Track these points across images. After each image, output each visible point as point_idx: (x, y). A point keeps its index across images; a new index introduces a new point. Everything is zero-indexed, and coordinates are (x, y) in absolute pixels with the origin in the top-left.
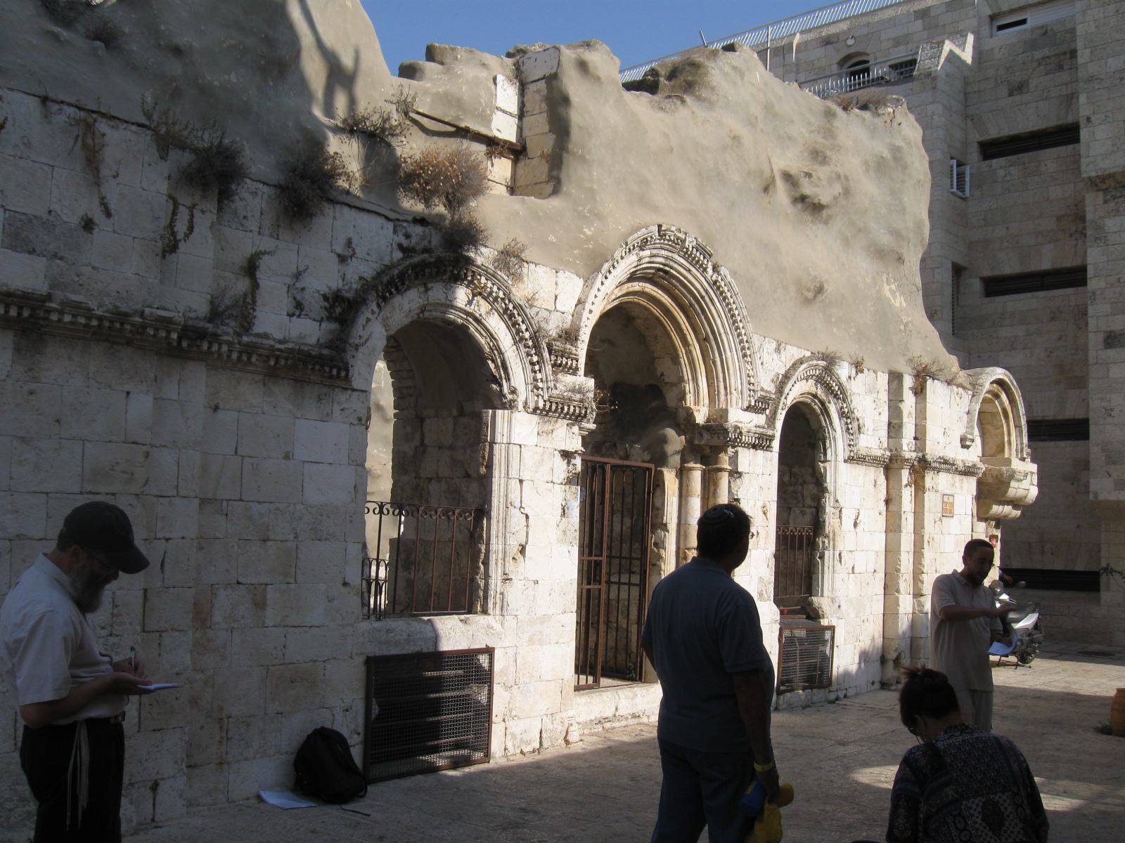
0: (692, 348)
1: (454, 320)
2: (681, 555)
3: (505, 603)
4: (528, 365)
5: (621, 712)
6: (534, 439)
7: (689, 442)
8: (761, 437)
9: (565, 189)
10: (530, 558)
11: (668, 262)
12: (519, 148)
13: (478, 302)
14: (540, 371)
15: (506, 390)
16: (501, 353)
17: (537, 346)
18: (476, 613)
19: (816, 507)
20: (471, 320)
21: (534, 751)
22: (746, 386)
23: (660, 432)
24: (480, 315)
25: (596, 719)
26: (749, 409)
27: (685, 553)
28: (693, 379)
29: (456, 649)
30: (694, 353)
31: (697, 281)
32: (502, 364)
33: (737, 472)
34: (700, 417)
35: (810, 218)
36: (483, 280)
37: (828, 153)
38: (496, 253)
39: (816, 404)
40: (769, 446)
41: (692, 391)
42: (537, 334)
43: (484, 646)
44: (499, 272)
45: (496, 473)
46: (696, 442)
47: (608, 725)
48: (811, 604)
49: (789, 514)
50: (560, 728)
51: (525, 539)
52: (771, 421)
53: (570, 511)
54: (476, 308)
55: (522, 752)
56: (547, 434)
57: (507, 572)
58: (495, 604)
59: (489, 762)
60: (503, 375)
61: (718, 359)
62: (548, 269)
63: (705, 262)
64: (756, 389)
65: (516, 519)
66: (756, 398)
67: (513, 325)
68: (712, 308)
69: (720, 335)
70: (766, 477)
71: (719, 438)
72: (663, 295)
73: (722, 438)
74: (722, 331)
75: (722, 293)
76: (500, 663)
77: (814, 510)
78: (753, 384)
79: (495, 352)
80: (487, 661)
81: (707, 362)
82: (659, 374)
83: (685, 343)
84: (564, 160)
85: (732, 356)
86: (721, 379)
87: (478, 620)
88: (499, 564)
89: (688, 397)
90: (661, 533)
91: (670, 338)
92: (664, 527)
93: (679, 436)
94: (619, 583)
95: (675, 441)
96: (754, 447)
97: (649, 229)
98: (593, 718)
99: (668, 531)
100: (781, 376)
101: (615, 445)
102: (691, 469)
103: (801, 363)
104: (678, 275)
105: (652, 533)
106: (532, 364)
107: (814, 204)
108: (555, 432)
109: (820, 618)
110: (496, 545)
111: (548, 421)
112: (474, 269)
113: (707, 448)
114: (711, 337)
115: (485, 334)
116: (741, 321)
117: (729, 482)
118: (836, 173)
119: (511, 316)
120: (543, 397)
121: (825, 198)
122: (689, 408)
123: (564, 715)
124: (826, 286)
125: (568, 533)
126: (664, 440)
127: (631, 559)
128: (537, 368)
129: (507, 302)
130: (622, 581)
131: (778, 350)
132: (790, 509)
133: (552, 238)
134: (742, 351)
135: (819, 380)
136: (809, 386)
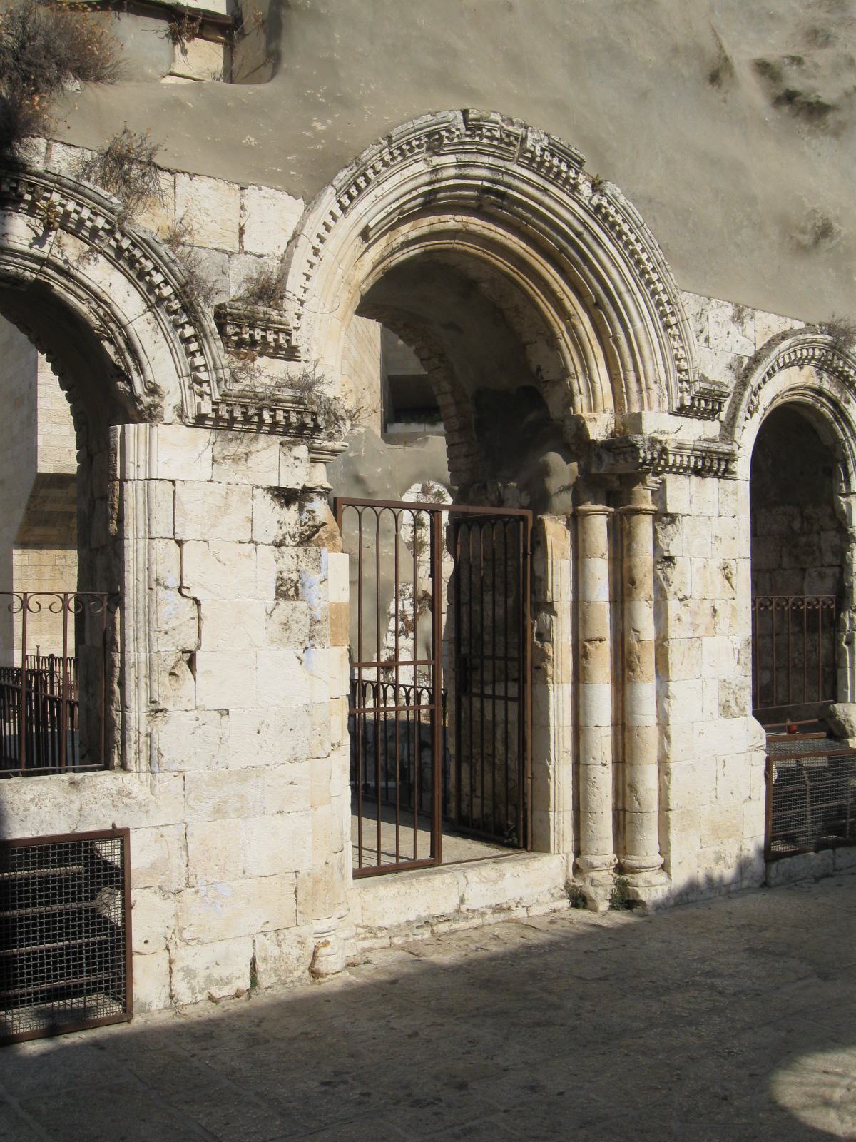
0: (577, 322)
1: (18, 275)
2: (581, 652)
3: (155, 753)
4: (178, 344)
5: (472, 903)
6: (206, 470)
7: (584, 471)
8: (706, 455)
9: (285, 65)
11: (499, 177)
12: (230, 22)
13: (58, 239)
14: (201, 351)
15: (139, 389)
16: (121, 326)
17: (189, 309)
18: (112, 768)
20: (50, 272)
21: (238, 995)
23: (541, 460)
24: (66, 262)
25: (419, 918)
26: (681, 411)
27: (585, 647)
28: (584, 371)
29: (41, 834)
30: (580, 327)
31: (565, 209)
32: (127, 344)
33: (667, 515)
34: (599, 428)
35: (805, 127)
36: (56, 197)
37: (833, 30)
38: (96, 155)
39: (823, 405)
40: (726, 470)
41: (583, 389)
42: (188, 289)
43: (108, 827)
44: (85, 183)
45: (130, 532)
46: (594, 471)
47: (443, 928)
48: (833, 715)
49: (804, 578)
50: (296, 952)
51: (194, 639)
52: (728, 429)
53: (307, 591)
54: (55, 250)
55: (211, 998)
56: (236, 459)
57: (156, 698)
58: (138, 753)
60: (131, 364)
61: (621, 335)
62: (221, 184)
63: (572, 174)
65: (171, 609)
67: (139, 277)
69: (620, 295)
70: (727, 520)
71: (625, 459)
72: (509, 235)
73: (630, 460)
74: (622, 288)
75: (613, 225)
76: (142, 857)
77: (837, 570)
78: (686, 371)
79: (112, 325)
80: (117, 851)
82: (534, 369)
83: (564, 314)
84: (284, 21)
85: (643, 325)
86: (630, 367)
87: (104, 781)
88: (142, 685)
89: (577, 399)
90: (545, 616)
92: (550, 608)
93: (568, 461)
94: (494, 697)
95: (562, 471)
96: (697, 472)
97: (440, 115)
98: (413, 918)
99: (555, 614)
100: (746, 361)
101: (485, 487)
102: (587, 514)
103: (783, 339)
104: (524, 199)
106: (186, 341)
107: (810, 104)
108: (252, 458)
110: (135, 654)
111: (237, 438)
112: (33, 179)
113: (614, 478)
115: (85, 296)
116: (653, 270)
117: (655, 531)
119: (132, 261)
120: (210, 395)
121: (828, 94)
122: (580, 417)
123: (304, 930)
125: (294, 626)
126: (545, 471)
127: (506, 658)
129: (118, 236)
130: (497, 694)
131: (738, 318)
132: (804, 570)
133: (251, 140)
135: (823, 366)
136: (806, 376)
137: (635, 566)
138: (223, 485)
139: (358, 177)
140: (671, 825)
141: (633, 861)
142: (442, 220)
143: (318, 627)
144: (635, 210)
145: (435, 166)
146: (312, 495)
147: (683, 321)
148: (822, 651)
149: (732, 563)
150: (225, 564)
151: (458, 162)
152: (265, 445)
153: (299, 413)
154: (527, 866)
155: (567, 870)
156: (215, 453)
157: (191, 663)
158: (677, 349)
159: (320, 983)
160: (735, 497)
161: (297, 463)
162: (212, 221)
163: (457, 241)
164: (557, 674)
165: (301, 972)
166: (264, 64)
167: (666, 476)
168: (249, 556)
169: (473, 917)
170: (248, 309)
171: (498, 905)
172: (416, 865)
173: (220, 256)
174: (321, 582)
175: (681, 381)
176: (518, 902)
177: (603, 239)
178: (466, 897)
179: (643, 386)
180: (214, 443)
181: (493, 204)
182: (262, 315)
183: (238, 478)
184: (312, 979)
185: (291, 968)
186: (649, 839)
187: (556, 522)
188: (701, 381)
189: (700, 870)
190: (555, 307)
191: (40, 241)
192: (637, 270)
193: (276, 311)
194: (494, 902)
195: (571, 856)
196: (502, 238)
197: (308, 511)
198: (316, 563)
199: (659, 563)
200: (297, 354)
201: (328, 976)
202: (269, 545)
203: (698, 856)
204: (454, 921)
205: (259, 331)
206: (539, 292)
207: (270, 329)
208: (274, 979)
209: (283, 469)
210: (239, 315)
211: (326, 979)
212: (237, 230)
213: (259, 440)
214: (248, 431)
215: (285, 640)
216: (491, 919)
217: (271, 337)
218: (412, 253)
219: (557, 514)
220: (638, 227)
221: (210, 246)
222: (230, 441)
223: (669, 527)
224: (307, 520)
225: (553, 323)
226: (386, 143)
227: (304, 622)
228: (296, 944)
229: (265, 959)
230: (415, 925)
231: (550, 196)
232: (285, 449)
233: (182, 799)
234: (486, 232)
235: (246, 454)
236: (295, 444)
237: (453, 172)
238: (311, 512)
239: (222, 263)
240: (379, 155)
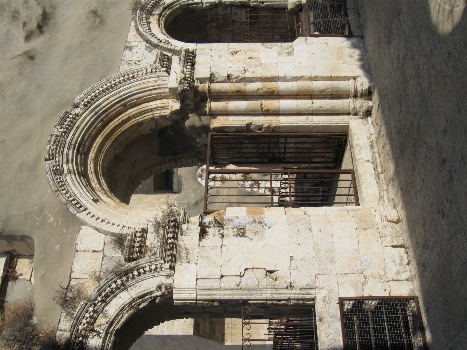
0: (132, 114)
1: (112, 343)
2: (267, 113)
3: (308, 287)
4: (141, 277)
5: (369, 157)
6: (192, 266)
7: (192, 111)
8: (186, 61)
10: (275, 265)
11: (72, 146)
13: (98, 326)
14: (144, 268)
15: (159, 293)
16: (133, 300)
17: (126, 273)
18: (314, 304)
19: (231, 7)
20: (111, 329)
21: (407, 253)
22: (153, 75)
24: (107, 323)
25: (375, 179)
26: (168, 72)
27: (264, 111)
28: (152, 111)
29: (341, 333)
30: (134, 113)
31: (85, 119)
32: (141, 298)
33: (211, 77)
34: (175, 105)
36: (81, 327)
37: (12, 9)
38: (63, 311)
39: (166, 13)
40: (192, 53)
41: (159, 112)
42: (118, 273)
43: (338, 306)
45: (218, 297)
46: (192, 107)
47: (379, 169)
48: (292, 10)
49: (237, 21)
50: (389, 229)
51: (261, 271)
52: (176, 52)
54: (102, 327)
55: (408, 264)
56: (188, 254)
57: (285, 286)
58: (308, 294)
59: (418, 297)
60: (149, 296)
62: (75, 260)
63: (71, 116)
64: (155, 67)
65: (249, 280)
67: (113, 293)
69: (121, 97)
71: (188, 94)
72: (96, 142)
73: (188, 93)
74: (118, 96)
75: (92, 99)
77: (233, 8)
78: (152, 69)
79: (133, 304)
80: (348, 302)
81: (139, 103)
82: (151, 131)
83: (129, 119)
84: (8, 234)
85: (133, 87)
86: (150, 92)
87: (319, 308)
88: (280, 292)
89: (163, 114)
90: (252, 127)
91: (125, 131)
92: (248, 125)
93: (189, 118)
94: (285, 148)
96: (193, 65)
98: (375, 181)
99: (251, 123)
100: (148, 45)
101: (199, 152)
102: (210, 110)
103: (138, 30)
104: (81, 136)
105: (253, 131)
106: (139, 274)
107: (43, 19)
108: (187, 247)
109: (301, 3)
110: (267, 295)
111: (179, 253)
112: (73, 337)
113: (196, 99)
114: (123, 102)
115: (121, 315)
117: (217, 82)
118: (23, 4)
119: (107, 296)
120: (162, 264)
121: (39, 12)
122: (171, 113)
123: (380, 226)
124: (92, 8)
125: (256, 230)
126: (193, 127)
127: (269, 143)
128: (142, 271)
129: (96, 302)
131: (130, 48)
132: (233, 21)
133: (57, 248)
135: (150, 13)
136: (154, 20)
139: (73, 204)
141: (352, 91)
142: (90, 169)
143: (256, 220)
144: (86, 90)
145: (68, 172)
146: (202, 223)
148: (266, 14)
149: (230, 51)
151: (66, 163)
152: (182, 242)
153: (169, 228)
155: (356, 118)
157: (271, 272)
158: (143, 73)
159: (402, 219)
160: (203, 49)
161: (189, 228)
163: (99, 163)
165: (397, 227)
166: (26, 242)
167: (195, 78)
168: (228, 248)
169: (375, 156)
171: (370, 146)
173: (105, 260)
174: (238, 219)
175: (156, 72)
176: (369, 138)
178: (367, 160)
179: (158, 87)
180: (181, 263)
181: (83, 149)
182: (129, 243)
183: (196, 253)
184: (400, 223)
185: (396, 231)
187: (213, 123)
188: (156, 63)
190: (126, 123)
191: (98, 334)
192: (111, 90)
193: (127, 237)
194: (369, 148)
196: (97, 145)
197: (209, 224)
198: (230, 221)
199: (230, 81)
200: (145, 229)
201: (399, 216)
202: (223, 240)
203: (350, 65)
205: (135, 244)
206: (120, 130)
207: (134, 240)
208: (400, 238)
209: (192, 234)
215: (262, 234)
217: (138, 239)
218: (104, 182)
221: (101, 264)
222: (180, 256)
224: (213, 224)
225: (132, 124)
226: (58, 192)
227: (255, 226)
228: (386, 229)
229: (392, 242)
230: (378, 180)
231: (80, 125)
232: (184, 233)
233: (327, 276)
234: (95, 151)
235: (186, 249)
236: (181, 229)
237: (70, 165)
238: (209, 223)
240: (63, 195)
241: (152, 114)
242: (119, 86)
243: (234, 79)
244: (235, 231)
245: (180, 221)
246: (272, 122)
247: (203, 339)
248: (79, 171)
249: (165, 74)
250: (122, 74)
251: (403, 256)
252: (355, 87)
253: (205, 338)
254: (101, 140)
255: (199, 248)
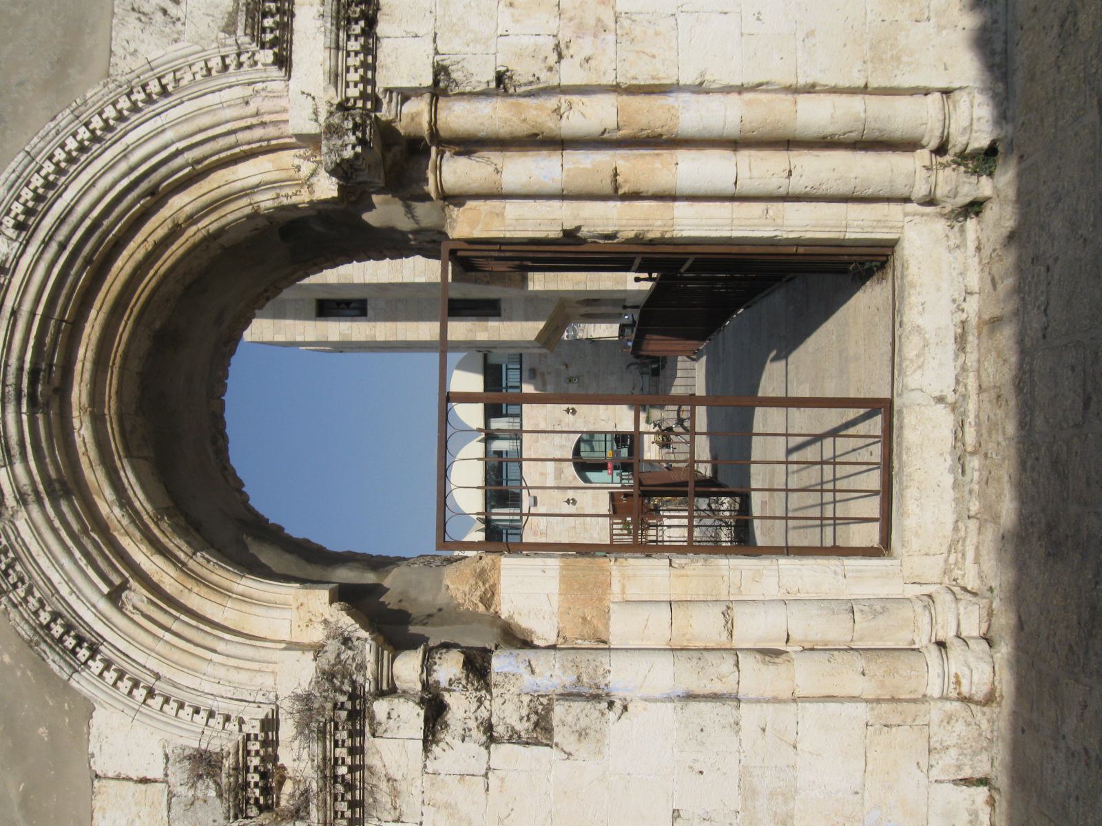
5: (945, 385)
22: (233, 77)
25: (952, 470)
26: (283, 62)
33: (436, 82)
47: (970, 436)
50: (959, 727)
56: (395, 793)
62: (97, 803)
66: (254, 47)
68: (80, 209)
69: (132, 169)
74: (123, 167)
78: (223, 58)
83: (176, 231)
86: (231, 139)
108: (394, 773)
111: (372, 792)
113: (390, 156)
114: (144, 186)
125: (583, 723)
134: (154, 102)
137: (511, 134)
138: (425, 809)
139: (52, 637)
140: (889, 86)
142: (83, 449)
144: (9, 169)
145: (18, 501)
146: (431, 682)
147: (152, 69)
150: (512, 810)
151: (5, 466)
152: (377, 757)
153: (336, 728)
154: (913, 286)
155: (927, 215)
156: (390, 818)
158: (194, 74)
159: (1001, 696)
161: (394, 715)
162: (140, 817)
163: (106, 411)
164: (660, 226)
165: (982, 717)
167: (379, 90)
168: (502, 780)
169: (965, 386)
170: (226, 796)
171: (956, 339)
172: (888, 437)
173: (176, 809)
174: (533, 672)
175: (240, 65)
176: (958, 307)
177: (60, 210)
178: (937, 394)
179: (254, 121)
180: (379, 820)
181: (48, 381)
182: (232, 779)
183: (416, 791)
184: (994, 705)
185: (976, 734)
186: (900, 116)
187: (455, 221)
188: (235, 33)
189: (960, 26)
190: (167, 247)
192: (94, 148)
193: (224, 761)
194: (951, 347)
195: (910, 207)
196: (89, 349)
197: (450, 685)
198: (511, 676)
199: (505, 89)
200: (270, 716)
201: (996, 683)
202: (489, 753)
203: (940, 28)
204: (964, 413)
205: (249, 776)
206: (152, 272)
207: (245, 763)
208: (984, 757)
209: (403, 734)
210: (235, 806)
211: (999, 687)
212: (142, 787)
213: (372, 765)
214: (363, 780)
215: (598, 736)
216: (972, 358)
217: (255, 761)
219: (444, 218)
220: (33, 159)
221: (166, 819)
222: (375, 800)
223: (454, 75)
224: (461, 686)
225: (188, 244)
227: (579, 710)
228: (949, 727)
229: (959, 768)
230: (960, 476)
231: (20, 304)
232: (380, 730)
234: (87, 376)
235: (388, 780)
236: (373, 718)
237: (19, 468)
238: (451, 682)
239: (182, 805)
240: (20, 608)
241: (251, 204)
242: (119, 129)
243: (520, 86)
244: (525, 704)
245: (367, 690)
246: (647, 226)
247: (477, 286)
248: (49, 477)
249: (275, 72)
250: (121, 87)
251: (981, 813)
252: (943, 132)
253: (480, 284)
254: (97, 329)
255: (425, 775)
